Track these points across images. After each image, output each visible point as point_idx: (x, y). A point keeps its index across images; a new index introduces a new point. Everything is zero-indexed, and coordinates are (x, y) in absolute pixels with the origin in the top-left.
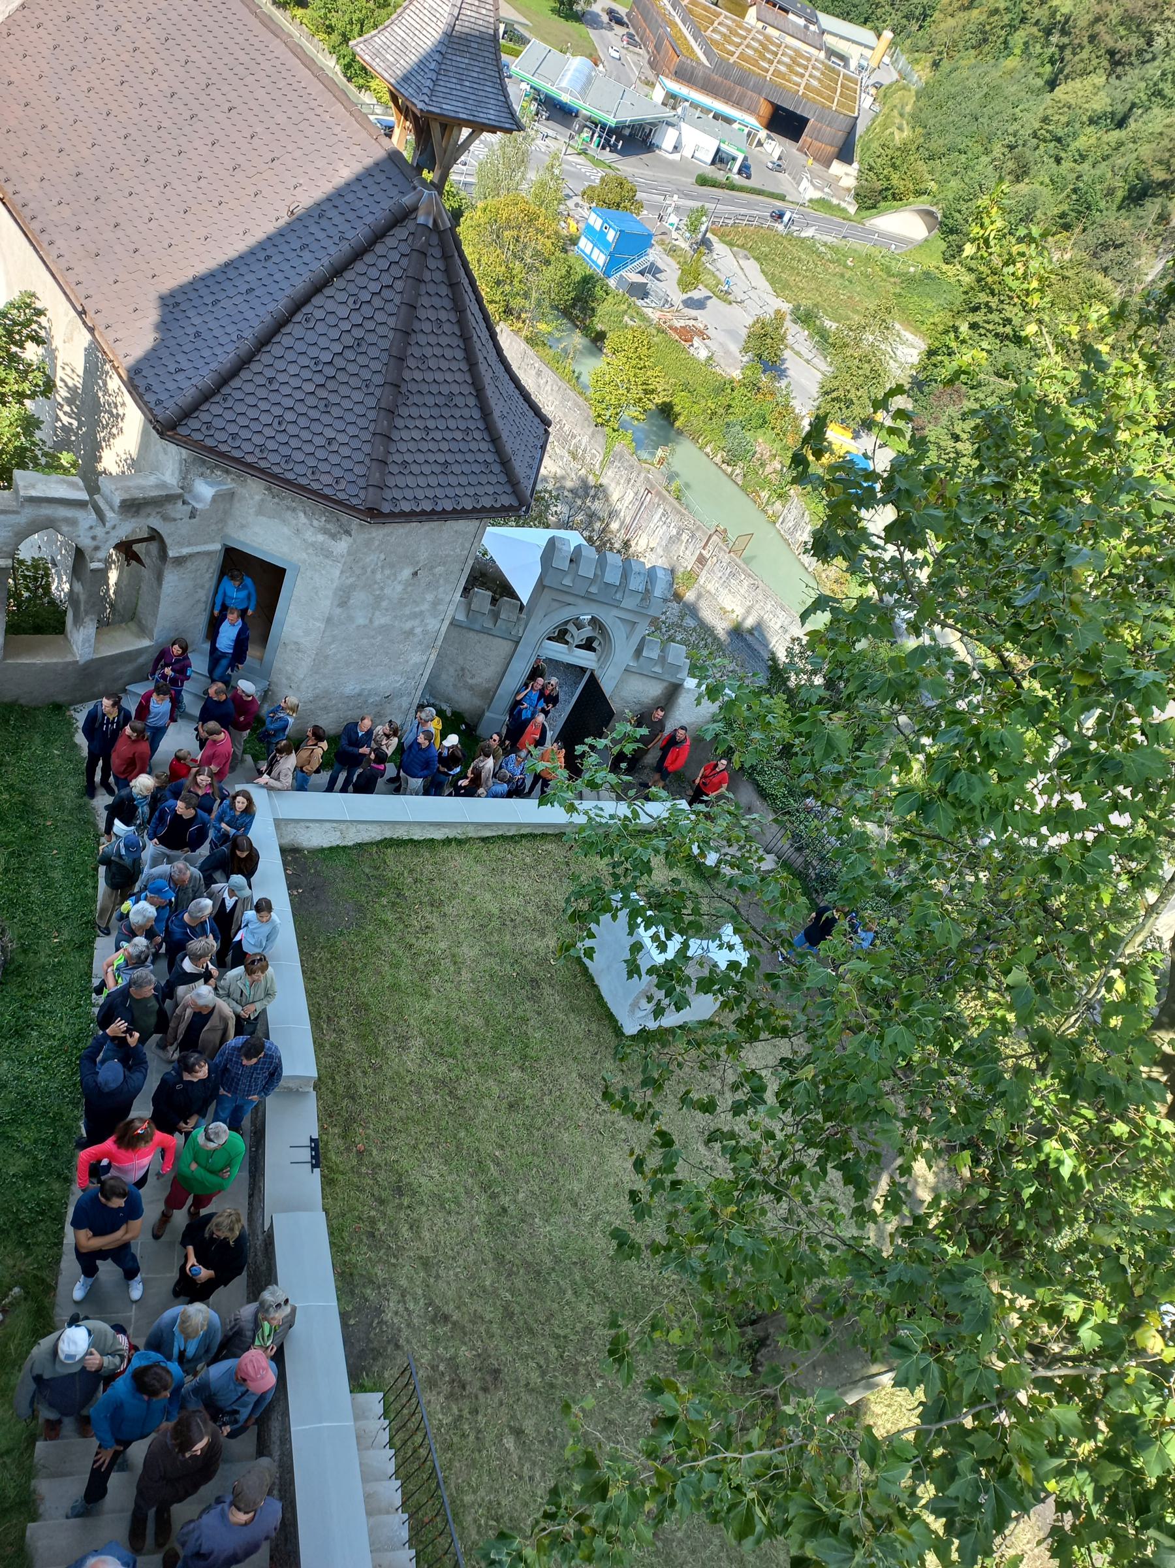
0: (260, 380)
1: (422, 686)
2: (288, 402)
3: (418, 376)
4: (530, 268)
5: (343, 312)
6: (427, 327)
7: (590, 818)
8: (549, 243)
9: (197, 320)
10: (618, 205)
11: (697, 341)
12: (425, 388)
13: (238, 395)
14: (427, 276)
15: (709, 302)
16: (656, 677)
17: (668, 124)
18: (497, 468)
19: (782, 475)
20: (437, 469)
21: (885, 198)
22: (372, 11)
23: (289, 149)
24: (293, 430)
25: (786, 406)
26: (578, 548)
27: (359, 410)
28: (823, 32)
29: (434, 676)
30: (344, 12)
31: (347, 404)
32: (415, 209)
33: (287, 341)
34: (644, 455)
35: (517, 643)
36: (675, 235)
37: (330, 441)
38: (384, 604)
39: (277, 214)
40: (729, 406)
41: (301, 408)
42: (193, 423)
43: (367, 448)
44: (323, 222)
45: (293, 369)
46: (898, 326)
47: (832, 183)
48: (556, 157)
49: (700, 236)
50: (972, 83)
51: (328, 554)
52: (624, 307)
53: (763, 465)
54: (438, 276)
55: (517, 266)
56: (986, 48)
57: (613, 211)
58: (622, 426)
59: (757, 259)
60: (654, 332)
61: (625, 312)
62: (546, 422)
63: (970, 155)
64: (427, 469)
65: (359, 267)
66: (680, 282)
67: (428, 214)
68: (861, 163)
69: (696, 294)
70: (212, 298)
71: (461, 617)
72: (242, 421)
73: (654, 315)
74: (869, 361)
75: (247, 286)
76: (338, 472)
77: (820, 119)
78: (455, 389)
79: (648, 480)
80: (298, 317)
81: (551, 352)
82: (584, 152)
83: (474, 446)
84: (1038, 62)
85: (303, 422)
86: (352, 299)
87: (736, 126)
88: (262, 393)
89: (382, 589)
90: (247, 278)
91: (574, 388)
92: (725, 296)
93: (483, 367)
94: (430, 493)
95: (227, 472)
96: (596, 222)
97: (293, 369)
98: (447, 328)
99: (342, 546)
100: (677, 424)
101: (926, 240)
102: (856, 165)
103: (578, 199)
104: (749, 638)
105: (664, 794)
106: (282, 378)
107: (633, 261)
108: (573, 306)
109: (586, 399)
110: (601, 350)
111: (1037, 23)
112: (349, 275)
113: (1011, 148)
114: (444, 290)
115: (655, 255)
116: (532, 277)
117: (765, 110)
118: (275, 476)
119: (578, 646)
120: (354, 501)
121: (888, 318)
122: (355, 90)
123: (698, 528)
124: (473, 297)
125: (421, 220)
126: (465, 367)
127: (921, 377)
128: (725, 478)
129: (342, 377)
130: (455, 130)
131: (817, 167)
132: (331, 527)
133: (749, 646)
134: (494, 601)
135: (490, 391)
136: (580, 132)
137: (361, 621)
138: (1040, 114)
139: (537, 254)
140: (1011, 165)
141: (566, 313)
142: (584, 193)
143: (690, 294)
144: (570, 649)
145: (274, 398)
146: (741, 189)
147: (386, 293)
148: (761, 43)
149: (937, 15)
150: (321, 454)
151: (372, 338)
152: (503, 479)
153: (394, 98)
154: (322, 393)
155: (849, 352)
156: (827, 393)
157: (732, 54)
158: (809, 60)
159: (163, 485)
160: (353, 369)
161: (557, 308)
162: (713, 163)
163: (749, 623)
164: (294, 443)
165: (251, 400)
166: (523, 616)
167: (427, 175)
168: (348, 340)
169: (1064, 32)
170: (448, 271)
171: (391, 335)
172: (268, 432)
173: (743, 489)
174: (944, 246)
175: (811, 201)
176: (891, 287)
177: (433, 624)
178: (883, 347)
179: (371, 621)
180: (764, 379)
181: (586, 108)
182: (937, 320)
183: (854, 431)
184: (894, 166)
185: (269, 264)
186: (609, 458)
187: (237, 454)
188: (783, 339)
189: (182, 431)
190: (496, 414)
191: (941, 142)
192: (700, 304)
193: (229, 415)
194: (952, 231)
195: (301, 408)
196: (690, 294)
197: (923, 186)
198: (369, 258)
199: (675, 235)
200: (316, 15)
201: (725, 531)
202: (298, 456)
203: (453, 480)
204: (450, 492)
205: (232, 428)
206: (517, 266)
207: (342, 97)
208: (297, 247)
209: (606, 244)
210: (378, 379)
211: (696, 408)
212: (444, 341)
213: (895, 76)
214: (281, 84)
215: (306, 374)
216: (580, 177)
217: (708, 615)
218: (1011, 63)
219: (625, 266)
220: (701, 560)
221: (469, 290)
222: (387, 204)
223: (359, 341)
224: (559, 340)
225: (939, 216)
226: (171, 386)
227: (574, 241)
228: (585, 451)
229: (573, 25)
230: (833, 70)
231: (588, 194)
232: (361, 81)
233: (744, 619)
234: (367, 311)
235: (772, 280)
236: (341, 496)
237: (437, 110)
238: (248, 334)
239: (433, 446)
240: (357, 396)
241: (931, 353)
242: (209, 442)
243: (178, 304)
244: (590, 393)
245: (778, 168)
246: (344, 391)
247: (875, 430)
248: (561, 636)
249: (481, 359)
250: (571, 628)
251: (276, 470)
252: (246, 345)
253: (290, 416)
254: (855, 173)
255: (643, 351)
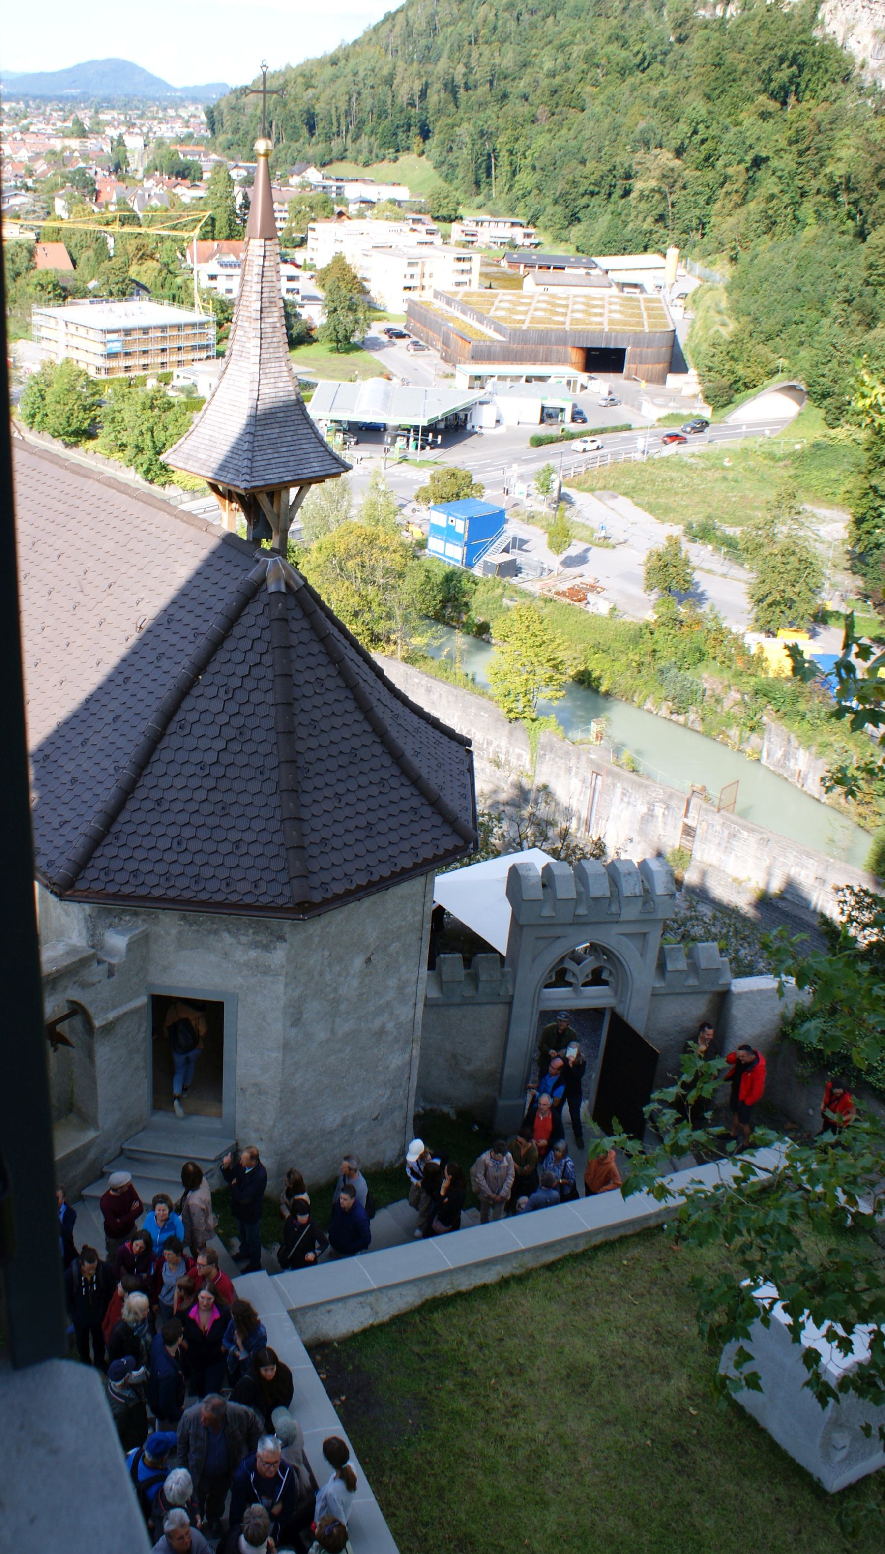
0: (149, 805)
1: (413, 1093)
2: (183, 818)
3: (313, 743)
4: (385, 588)
5: (216, 706)
6: (308, 690)
7: (688, 1196)
8: (397, 557)
9: (70, 766)
10: (458, 495)
11: (591, 597)
12: (323, 753)
13: (129, 828)
14: (294, 640)
15: (590, 555)
16: (695, 992)
17: (481, 403)
18: (427, 811)
19: (746, 704)
20: (361, 835)
21: (738, 391)
22: (159, 417)
23: (123, 570)
24: (194, 846)
25: (719, 630)
26: (547, 868)
27: (259, 800)
28: (607, 272)
29: (424, 1075)
30: (133, 428)
31: (245, 799)
32: (264, 580)
33: (166, 756)
34: (577, 735)
35: (510, 1004)
36: (527, 502)
37: (237, 844)
38: (343, 1007)
39: (126, 635)
40: (654, 651)
41: (198, 820)
42: (90, 874)
43: (278, 839)
44: (175, 626)
45: (180, 782)
46: (808, 507)
47: (676, 395)
48: (377, 474)
49: (555, 494)
50: (778, 261)
51: (266, 970)
52: (499, 591)
53: (718, 701)
54: (306, 636)
55: (371, 590)
56: (778, 229)
57: (454, 503)
58: (541, 712)
59: (625, 494)
60: (541, 604)
61: (502, 595)
62: (465, 742)
63: (808, 322)
64: (350, 839)
65: (222, 656)
66: (551, 545)
67: (278, 580)
68: (697, 366)
69: (573, 551)
70: (81, 739)
71: (434, 994)
72: (140, 854)
73: (535, 588)
74: (793, 553)
75: (113, 715)
76: (254, 875)
77: (637, 343)
78: (357, 743)
79: (591, 761)
80: (172, 727)
81: (435, 663)
82: (404, 459)
83: (394, 796)
84: (837, 222)
85: (204, 833)
86: (222, 690)
87: (550, 381)
88: (153, 818)
89: (336, 990)
90: (110, 707)
91: (472, 692)
92: (606, 542)
93: (379, 710)
94: (361, 864)
95: (136, 914)
96: (439, 519)
97: (180, 782)
98: (330, 683)
99: (279, 956)
100: (603, 689)
101: (800, 414)
102: (692, 371)
103: (414, 505)
104: (781, 904)
105: (772, 1134)
106: (170, 795)
107: (492, 542)
108: (444, 607)
109: (491, 698)
110: (488, 642)
111: (818, 192)
112: (213, 667)
113: (849, 302)
114: (316, 648)
115: (513, 529)
116: (391, 596)
117: (576, 356)
118: (189, 902)
119: (585, 985)
120: (280, 901)
121: (793, 502)
122: (160, 489)
123: (671, 796)
124: (347, 643)
125: (272, 588)
126: (359, 716)
127: (858, 550)
128: (681, 730)
129: (232, 773)
130: (283, 494)
131: (654, 387)
132: (263, 938)
133: (786, 914)
134: (467, 963)
135: (394, 732)
136: (394, 442)
137: (322, 1036)
138: (863, 263)
139: (388, 572)
140: (856, 317)
141: (439, 618)
142: (417, 498)
143: (566, 554)
144: (576, 991)
145: (168, 818)
146: (580, 435)
147: (256, 672)
148: (548, 303)
149: (713, 220)
150: (231, 861)
151: (253, 722)
152: (437, 820)
153: (214, 488)
154: (216, 796)
155: (765, 551)
156: (760, 601)
157: (523, 322)
158: (602, 299)
159: (73, 950)
160: (241, 760)
161: (427, 617)
162: (542, 421)
163: (776, 887)
164: (199, 859)
165: (144, 829)
166: (507, 969)
167: (266, 545)
168: (229, 732)
169: (849, 190)
170: (314, 628)
171: (273, 711)
172: (170, 856)
173: (706, 735)
174: (822, 413)
175: (659, 420)
176: (782, 472)
177: (405, 1013)
178: (801, 533)
179: (333, 1032)
180: (683, 611)
181: (392, 421)
182: (849, 487)
183: (809, 631)
184: (733, 359)
185: (129, 685)
186: (539, 753)
187: (142, 891)
188: (687, 563)
189: (81, 885)
190: (408, 753)
191: (772, 321)
192: (581, 559)
193: (125, 853)
194: (824, 396)
195: (198, 820)
196: (566, 554)
197: (772, 366)
198: (229, 644)
199: (527, 502)
200: (107, 440)
201: (704, 789)
202: (207, 872)
203: (382, 841)
204: (383, 855)
205: (131, 866)
206: (371, 590)
207: (149, 500)
208: (154, 659)
209: (458, 537)
210: (272, 762)
211: (617, 666)
212: (330, 697)
213: (697, 283)
214: (102, 516)
215: (195, 782)
216: (407, 484)
217: (721, 891)
218: (809, 232)
219: (486, 550)
220: (689, 831)
221: (341, 637)
222: (233, 587)
223: (241, 730)
224: (439, 648)
225: (803, 387)
226: (59, 842)
227: (422, 545)
228: (507, 753)
229: (355, 355)
230: (631, 299)
231: (423, 496)
232: (163, 479)
233: (768, 884)
234: (241, 696)
235: (650, 508)
236: (264, 900)
237: (262, 483)
238: (125, 762)
239: (348, 811)
240: (254, 787)
241: (859, 521)
242: (112, 889)
243: (47, 756)
244: (493, 691)
245: (612, 402)
246: (238, 786)
247: (832, 621)
248: (560, 978)
249: (375, 703)
250: (570, 965)
251: (188, 894)
252: (127, 772)
253: (188, 833)
254: (696, 379)
255: (535, 628)
